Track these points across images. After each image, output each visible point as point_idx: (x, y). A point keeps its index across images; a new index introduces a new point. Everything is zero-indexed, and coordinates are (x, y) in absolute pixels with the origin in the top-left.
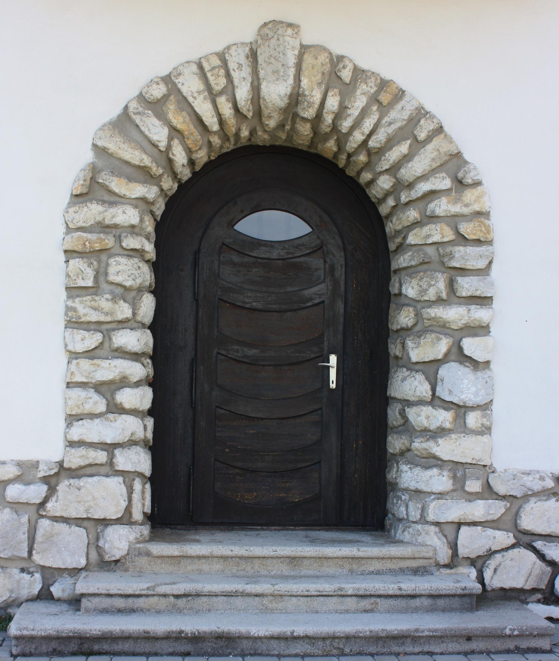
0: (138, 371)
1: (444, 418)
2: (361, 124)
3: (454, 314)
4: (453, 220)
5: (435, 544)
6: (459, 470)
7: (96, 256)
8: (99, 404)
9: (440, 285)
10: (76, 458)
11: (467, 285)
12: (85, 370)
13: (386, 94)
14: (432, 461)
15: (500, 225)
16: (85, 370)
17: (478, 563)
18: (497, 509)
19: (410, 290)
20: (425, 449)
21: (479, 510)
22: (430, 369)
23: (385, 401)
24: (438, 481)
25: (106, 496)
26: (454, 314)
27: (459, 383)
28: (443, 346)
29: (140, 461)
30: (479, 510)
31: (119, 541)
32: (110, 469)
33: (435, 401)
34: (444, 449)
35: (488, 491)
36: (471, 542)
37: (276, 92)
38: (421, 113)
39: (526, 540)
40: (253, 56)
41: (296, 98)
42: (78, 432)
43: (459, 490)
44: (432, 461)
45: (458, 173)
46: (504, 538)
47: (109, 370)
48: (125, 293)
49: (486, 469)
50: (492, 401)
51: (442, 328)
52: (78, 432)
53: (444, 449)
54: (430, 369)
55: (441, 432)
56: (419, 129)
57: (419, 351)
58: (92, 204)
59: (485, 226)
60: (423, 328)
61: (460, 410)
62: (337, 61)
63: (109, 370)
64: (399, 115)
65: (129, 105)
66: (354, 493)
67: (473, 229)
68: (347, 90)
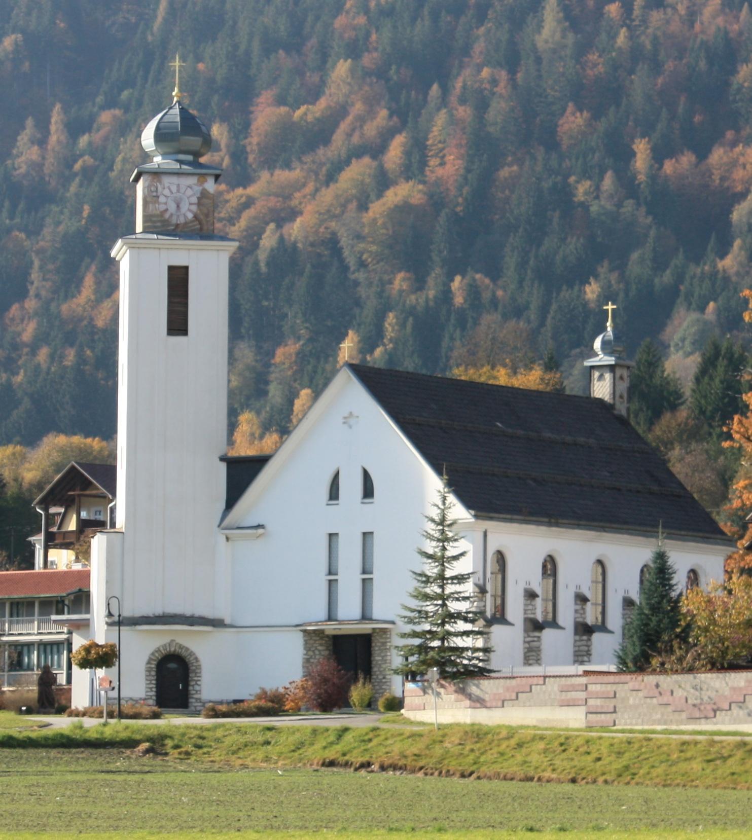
2: (184, 653)
6: (197, 699)
13: (187, 649)
27: (197, 688)
29: (154, 698)
37: (173, 649)
45: (197, 659)
49: (200, 699)
56: (192, 654)
67: (199, 667)
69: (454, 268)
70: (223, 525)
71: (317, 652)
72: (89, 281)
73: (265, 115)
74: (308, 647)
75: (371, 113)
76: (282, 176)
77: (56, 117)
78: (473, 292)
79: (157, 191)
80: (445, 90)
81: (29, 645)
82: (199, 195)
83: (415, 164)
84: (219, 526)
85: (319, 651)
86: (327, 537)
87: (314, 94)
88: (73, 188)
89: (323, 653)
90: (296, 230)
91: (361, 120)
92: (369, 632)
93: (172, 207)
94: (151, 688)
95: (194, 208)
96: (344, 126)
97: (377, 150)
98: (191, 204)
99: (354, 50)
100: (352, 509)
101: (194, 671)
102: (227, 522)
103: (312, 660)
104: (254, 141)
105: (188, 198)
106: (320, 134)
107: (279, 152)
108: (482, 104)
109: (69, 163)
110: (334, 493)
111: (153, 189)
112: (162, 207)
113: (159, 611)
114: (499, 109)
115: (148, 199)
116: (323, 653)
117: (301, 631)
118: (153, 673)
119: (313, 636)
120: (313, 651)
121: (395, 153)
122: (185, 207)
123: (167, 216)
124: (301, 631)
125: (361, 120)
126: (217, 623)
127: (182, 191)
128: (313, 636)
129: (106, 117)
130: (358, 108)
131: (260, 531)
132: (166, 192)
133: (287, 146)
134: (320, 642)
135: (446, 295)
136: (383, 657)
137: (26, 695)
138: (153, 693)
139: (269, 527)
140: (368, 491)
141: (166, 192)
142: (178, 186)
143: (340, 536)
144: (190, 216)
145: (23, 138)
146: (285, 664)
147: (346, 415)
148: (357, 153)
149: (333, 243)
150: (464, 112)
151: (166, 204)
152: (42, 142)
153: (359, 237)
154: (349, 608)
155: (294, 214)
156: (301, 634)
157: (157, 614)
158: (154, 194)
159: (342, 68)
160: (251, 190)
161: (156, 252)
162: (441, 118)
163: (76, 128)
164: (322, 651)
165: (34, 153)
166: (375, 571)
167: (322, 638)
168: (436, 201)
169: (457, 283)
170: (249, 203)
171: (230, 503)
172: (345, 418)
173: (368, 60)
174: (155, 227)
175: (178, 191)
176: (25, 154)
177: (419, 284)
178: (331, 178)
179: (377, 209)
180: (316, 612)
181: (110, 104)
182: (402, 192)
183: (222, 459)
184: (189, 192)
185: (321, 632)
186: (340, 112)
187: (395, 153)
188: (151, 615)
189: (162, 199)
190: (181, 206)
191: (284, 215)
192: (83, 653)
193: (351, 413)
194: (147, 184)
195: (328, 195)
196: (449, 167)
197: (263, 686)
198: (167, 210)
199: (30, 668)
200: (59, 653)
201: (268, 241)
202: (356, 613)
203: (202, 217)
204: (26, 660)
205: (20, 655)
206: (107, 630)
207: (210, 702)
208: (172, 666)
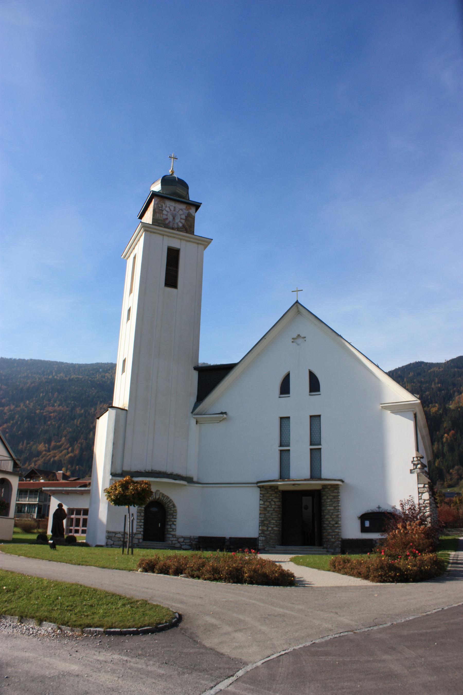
0: (143, 524)
1: (171, 530)
3: (173, 520)
4: (173, 510)
5: (170, 542)
6: (173, 535)
7: (140, 513)
8: (139, 527)
9: (172, 517)
10: (137, 532)
11: (174, 517)
12: (138, 524)
13: (168, 498)
14: (170, 534)
15: (178, 511)
16: (138, 524)
17: (175, 544)
18: (176, 539)
19: (169, 517)
20: (273, 563)
22: (170, 525)
24: (171, 536)
25: (140, 536)
26: (173, 520)
27: (173, 527)
28: (172, 523)
29: (142, 533)
30: (175, 539)
31: (141, 541)
32: (140, 534)
33: (171, 528)
34: (172, 533)
35: (175, 537)
36: (174, 542)
37: (157, 497)
38: (171, 500)
39: (179, 542)
40: (155, 494)
41: (159, 498)
42: (138, 530)
43: (173, 537)
44: (170, 534)
45: (174, 506)
46: (176, 542)
47: (141, 524)
48: (142, 516)
49: (175, 535)
51: (172, 521)
52: (138, 530)
53: (172, 533)
54: (170, 525)
55: (171, 531)
56: (171, 501)
57: (170, 523)
60: (170, 521)
61: (173, 529)
62: (163, 494)
63: (141, 524)
64: (169, 500)
65: (289, 560)
67: (175, 511)
68: (164, 497)
69: (77, 465)
70: (194, 413)
71: (273, 503)
72: (27, 463)
73: (53, 444)
74: (263, 498)
75: (67, 444)
76: (55, 451)
77: (25, 442)
78: (79, 468)
79: (162, 207)
80: (77, 443)
81: (25, 505)
82: (186, 215)
83: (72, 451)
84: (192, 413)
85: (274, 502)
86: (279, 419)
87: (60, 442)
88: (26, 451)
89: (277, 503)
90: (56, 458)
91: (66, 445)
92: (319, 488)
93: (170, 218)
94: (140, 526)
95: (183, 221)
96: (63, 446)
97: (68, 449)
98: (181, 219)
99: (65, 436)
100: (300, 404)
101: (172, 514)
102: (197, 410)
103: (268, 509)
104: (51, 447)
105: (180, 215)
106: (60, 446)
107: (54, 448)
108: (82, 444)
109: (26, 448)
110: (285, 388)
111: (160, 206)
112: (165, 217)
113: (149, 468)
114: (84, 445)
115: (156, 210)
116: (277, 503)
117: (259, 487)
118: (143, 514)
119: (266, 489)
120: (270, 502)
121: (70, 449)
122: (177, 220)
123: (167, 222)
125: (66, 445)
126: (190, 480)
127: (177, 210)
128: (266, 489)
129: (32, 443)
130: (65, 444)
131: (225, 416)
132: (167, 209)
133: (55, 448)
134: (275, 495)
135: (76, 468)
136: (335, 507)
137: (26, 522)
138: (142, 530)
139: (230, 413)
140: (314, 385)
141: (167, 209)
142: (175, 207)
143: (291, 419)
145: (20, 444)
147: (295, 337)
148: (65, 449)
149: (61, 461)
150: (79, 445)
151: (167, 215)
152: (23, 445)
153: (64, 460)
154: (300, 470)
155: (55, 456)
156: (258, 489)
157: (147, 471)
158: (161, 209)
159: (64, 438)
160: (51, 453)
161: (161, 237)
162: (76, 446)
163: (27, 444)
164: (276, 502)
165: (22, 446)
166: (322, 443)
167: (276, 493)
168: (75, 456)
169: (77, 467)
170: (50, 455)
172: (293, 339)
173: (67, 438)
175: (175, 210)
176: (20, 446)
177: (72, 466)
178: (61, 452)
179: (67, 456)
180: (271, 472)
181: (32, 441)
182: (70, 455)
184: (181, 212)
185: (276, 487)
186: (63, 444)
187: (70, 449)
188: (143, 471)
189: (165, 212)
190: (176, 218)
191: (54, 456)
192: (119, 489)
193: (299, 335)
194: (156, 202)
195: (61, 454)
196: (77, 452)
198: (167, 219)
199: (24, 512)
200: (35, 508)
201: (52, 460)
202: (307, 474)
203: (187, 227)
204: (23, 509)
205: (22, 508)
206: (111, 479)
207: (182, 537)
208: (154, 509)
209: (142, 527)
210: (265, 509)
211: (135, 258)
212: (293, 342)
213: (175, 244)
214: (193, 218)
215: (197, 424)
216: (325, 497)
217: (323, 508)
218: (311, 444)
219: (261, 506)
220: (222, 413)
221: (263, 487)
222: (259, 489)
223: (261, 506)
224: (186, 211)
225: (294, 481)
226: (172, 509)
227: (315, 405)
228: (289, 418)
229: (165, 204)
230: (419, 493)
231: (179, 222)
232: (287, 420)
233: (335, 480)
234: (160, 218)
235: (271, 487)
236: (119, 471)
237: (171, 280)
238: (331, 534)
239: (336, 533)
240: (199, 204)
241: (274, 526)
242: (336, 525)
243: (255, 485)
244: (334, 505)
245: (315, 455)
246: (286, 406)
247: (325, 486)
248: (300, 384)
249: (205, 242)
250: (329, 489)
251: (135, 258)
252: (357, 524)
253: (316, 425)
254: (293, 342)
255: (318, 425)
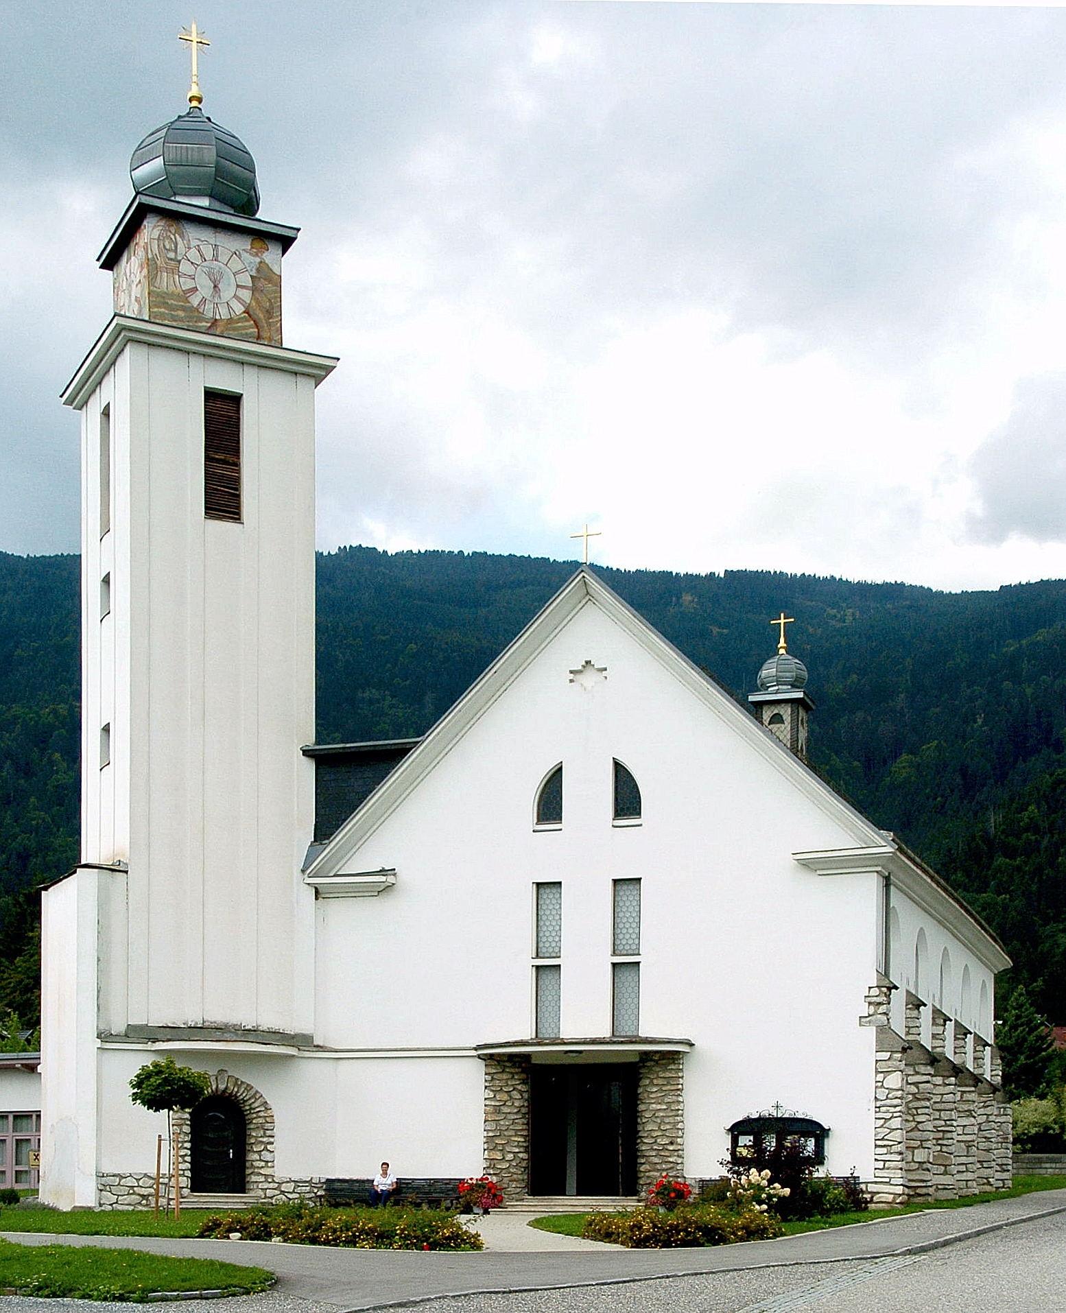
1: (263, 1164)
2: (242, 1094)
5: (261, 1193)
7: (180, 1125)
11: (268, 1133)
21: (271, 1185)
23: (245, 1161)
25: (185, 1182)
27: (267, 1156)
29: (188, 1173)
30: (271, 1185)
31: (186, 1192)
32: (183, 1175)
37: (222, 1087)
39: (283, 1192)
43: (266, 1181)
47: (182, 1153)
50: (618, 767)
58: (666, 1060)
59: (1027, 830)
64: (252, 1092)
66: (239, 1185)
74: (491, 1084)
95: (246, 295)
100: (589, 843)
101: (261, 1127)
110: (550, 805)
112: (188, 284)
117: (479, 1057)
118: (187, 1129)
122: (227, 292)
123: (195, 301)
124: (479, 1057)
127: (223, 258)
128: (506, 1063)
131: (391, 879)
132: (193, 254)
140: (627, 799)
144: (239, 309)
146: (448, 1130)
154: (584, 1020)
158: (172, 255)
171: (325, 828)
174: (174, 318)
180: (514, 1026)
183: (307, 753)
184: (236, 264)
185: (526, 1057)
189: (185, 267)
197: (227, 116)
209: (188, 1159)
210: (497, 1110)
211: (106, 413)
212: (571, 681)
213: (226, 379)
214: (277, 281)
215: (317, 899)
216: (647, 1082)
217: (641, 1107)
218: (614, 954)
219: (488, 1103)
220: (383, 872)
221: (491, 1056)
222: (482, 1063)
223: (488, 1103)
224: (252, 259)
225: (565, 1044)
226: (262, 1114)
227: (627, 848)
228: (560, 883)
229: (182, 237)
230: (877, 1072)
231: (232, 301)
232: (554, 891)
233: (669, 1042)
234: (172, 288)
235: (511, 1057)
236: (119, 1027)
237: (223, 499)
238: (658, 1167)
239: (669, 1166)
240: (290, 233)
241: (516, 1151)
242: (671, 1148)
243: (474, 1053)
244: (666, 1100)
245: (625, 970)
246: (550, 853)
247: (646, 1056)
248: (589, 795)
249: (315, 370)
250: (656, 1062)
251: (106, 413)
252: (721, 1147)
253: (624, 931)
254: (571, 681)
255: (634, 936)
